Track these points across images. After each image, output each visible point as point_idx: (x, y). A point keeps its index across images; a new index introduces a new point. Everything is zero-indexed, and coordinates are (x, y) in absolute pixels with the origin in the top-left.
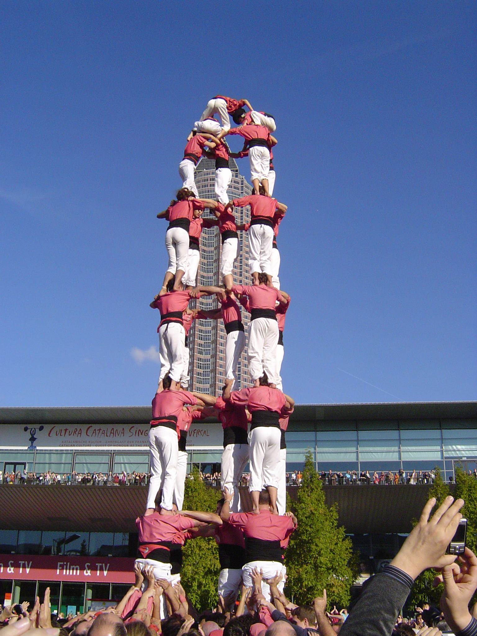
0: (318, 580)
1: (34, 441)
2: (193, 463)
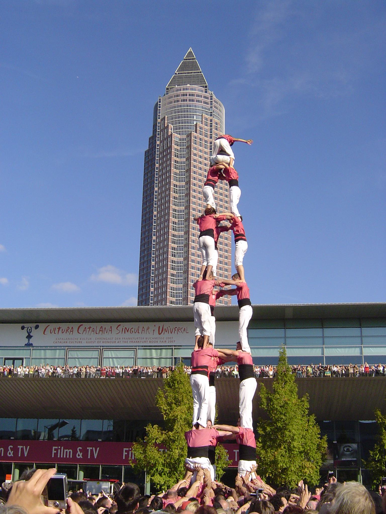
0: (292, 462)
1: (31, 338)
2: (174, 358)
